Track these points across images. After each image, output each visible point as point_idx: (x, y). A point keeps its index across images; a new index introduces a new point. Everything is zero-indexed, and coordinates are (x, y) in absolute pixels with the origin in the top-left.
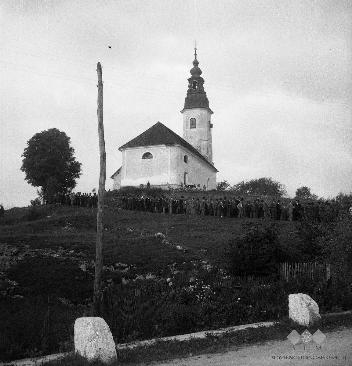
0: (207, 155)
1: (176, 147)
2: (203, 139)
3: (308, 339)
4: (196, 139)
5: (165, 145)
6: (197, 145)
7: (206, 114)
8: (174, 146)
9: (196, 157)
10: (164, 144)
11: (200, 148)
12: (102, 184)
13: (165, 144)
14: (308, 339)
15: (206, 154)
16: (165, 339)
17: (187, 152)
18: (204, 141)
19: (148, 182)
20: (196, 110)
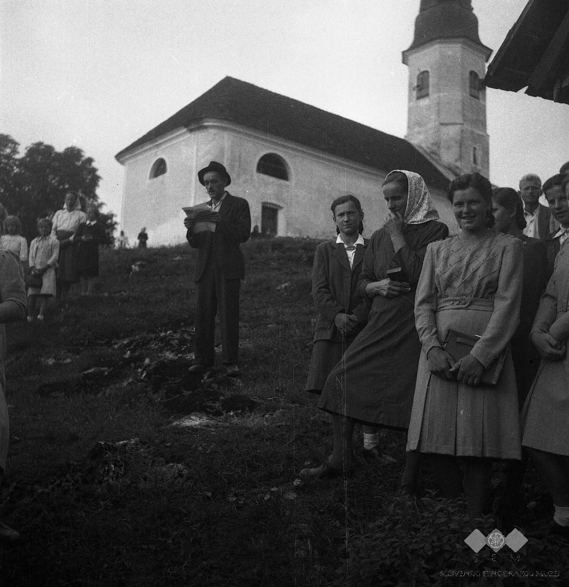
0: (458, 164)
1: (212, 131)
2: (446, 121)
3: (499, 544)
4: (429, 126)
5: (185, 130)
6: (431, 141)
7: (459, 55)
8: (206, 127)
9: (313, 153)
10: (181, 126)
11: (439, 147)
12: (483, 452)
13: (186, 126)
14: (499, 544)
15: (456, 161)
16: (85, 373)
17: (271, 142)
18: (450, 127)
19: (183, 208)
20: (423, 52)
